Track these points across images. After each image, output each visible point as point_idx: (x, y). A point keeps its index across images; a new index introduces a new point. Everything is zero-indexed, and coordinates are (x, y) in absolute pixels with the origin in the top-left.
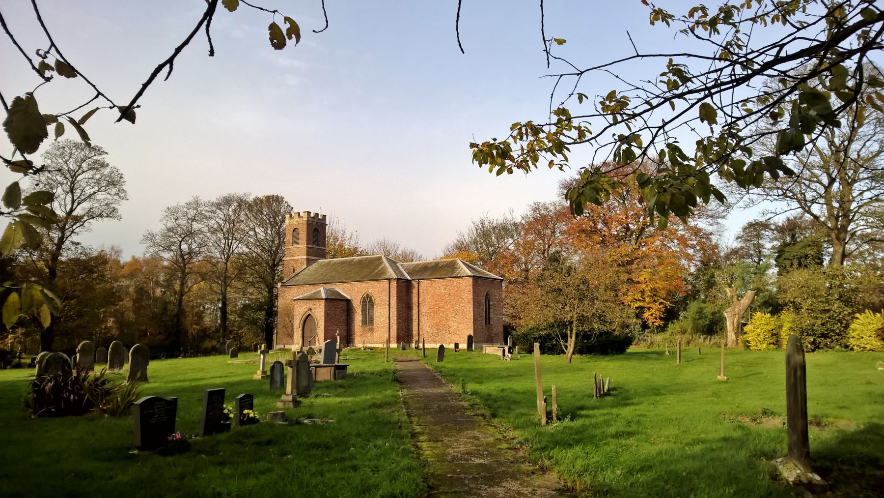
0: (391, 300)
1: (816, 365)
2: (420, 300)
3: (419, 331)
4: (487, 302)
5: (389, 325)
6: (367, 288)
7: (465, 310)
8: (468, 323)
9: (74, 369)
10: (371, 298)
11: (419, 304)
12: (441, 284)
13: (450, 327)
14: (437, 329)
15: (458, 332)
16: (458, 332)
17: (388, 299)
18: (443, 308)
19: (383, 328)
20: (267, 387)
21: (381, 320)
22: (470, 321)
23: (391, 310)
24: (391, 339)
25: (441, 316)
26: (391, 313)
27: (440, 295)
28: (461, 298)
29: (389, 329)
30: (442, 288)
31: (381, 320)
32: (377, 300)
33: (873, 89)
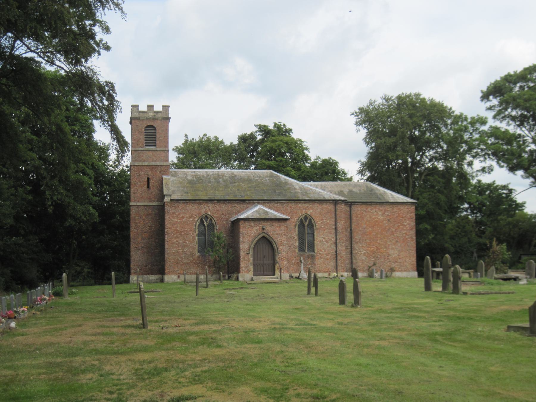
0: (338, 224)
1: (525, 321)
2: (353, 225)
3: (352, 259)
4: (342, 246)
5: (336, 252)
6: (305, 209)
7: (407, 237)
8: (411, 251)
9: (377, 272)
10: (310, 221)
11: (351, 230)
12: (379, 209)
13: (389, 255)
14: (374, 257)
15: (399, 261)
16: (399, 261)
17: (333, 223)
18: (382, 234)
19: (327, 255)
20: (142, 326)
21: (325, 246)
22: (412, 249)
23: (338, 234)
24: (339, 268)
25: (379, 243)
26: (338, 239)
27: (377, 221)
28: (402, 225)
29: (337, 257)
30: (380, 213)
31: (325, 246)
32: (318, 224)
33: (76, 29)
